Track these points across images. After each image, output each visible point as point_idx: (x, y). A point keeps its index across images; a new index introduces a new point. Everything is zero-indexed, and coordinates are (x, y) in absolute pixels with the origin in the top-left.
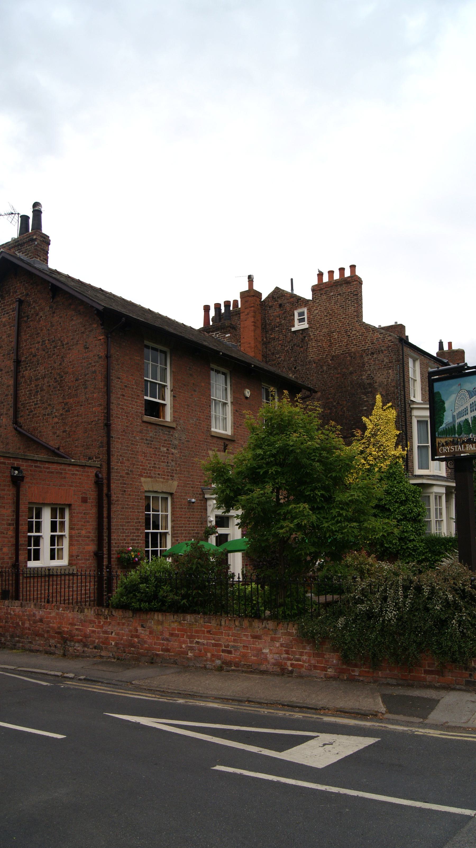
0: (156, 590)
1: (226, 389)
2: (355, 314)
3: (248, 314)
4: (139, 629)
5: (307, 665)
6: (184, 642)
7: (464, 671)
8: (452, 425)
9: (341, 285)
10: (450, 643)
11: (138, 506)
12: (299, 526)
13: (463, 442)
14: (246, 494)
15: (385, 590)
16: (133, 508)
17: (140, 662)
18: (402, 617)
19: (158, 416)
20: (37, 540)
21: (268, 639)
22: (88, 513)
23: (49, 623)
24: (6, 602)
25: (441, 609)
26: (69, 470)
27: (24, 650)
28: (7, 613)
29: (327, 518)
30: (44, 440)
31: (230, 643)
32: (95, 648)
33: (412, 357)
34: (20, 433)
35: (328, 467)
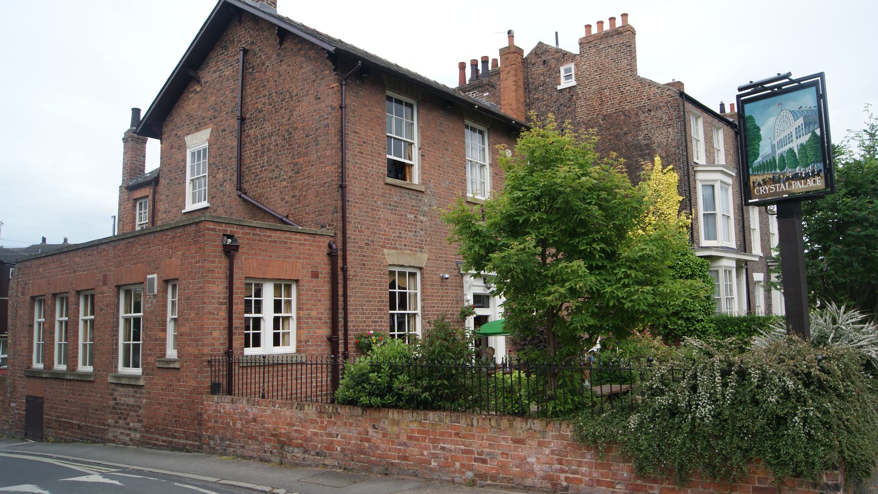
0: (391, 380)
1: (484, 150)
2: (629, 67)
3: (508, 73)
4: (370, 430)
5: (587, 479)
6: (426, 448)
7: (811, 490)
8: (771, 157)
9: (612, 36)
10: (792, 451)
11: (380, 282)
12: (572, 291)
13: (788, 179)
14: (501, 250)
15: (695, 377)
16: (375, 285)
17: (371, 472)
18: (720, 414)
19: (404, 179)
20: (257, 323)
21: (535, 444)
22: (320, 291)
23: (264, 422)
24: (216, 397)
25: (778, 402)
26: (295, 239)
27: (236, 455)
28: (216, 411)
29: (610, 281)
30: (272, 208)
31: (485, 450)
32: (317, 454)
33: (694, 115)
34: (245, 200)
35: (609, 214)
